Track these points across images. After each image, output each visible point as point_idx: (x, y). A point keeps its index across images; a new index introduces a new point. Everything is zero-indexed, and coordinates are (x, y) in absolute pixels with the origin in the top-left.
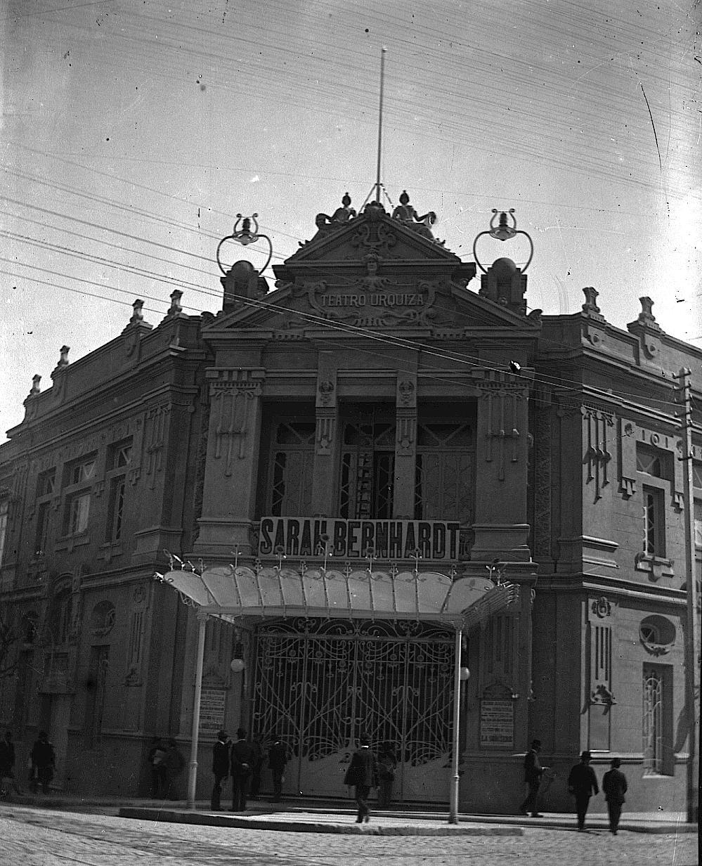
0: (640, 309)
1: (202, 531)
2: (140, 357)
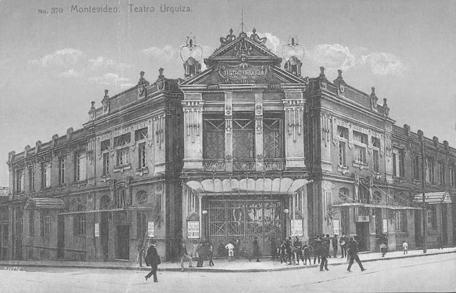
0: (320, 72)
1: (185, 163)
2: (146, 95)
